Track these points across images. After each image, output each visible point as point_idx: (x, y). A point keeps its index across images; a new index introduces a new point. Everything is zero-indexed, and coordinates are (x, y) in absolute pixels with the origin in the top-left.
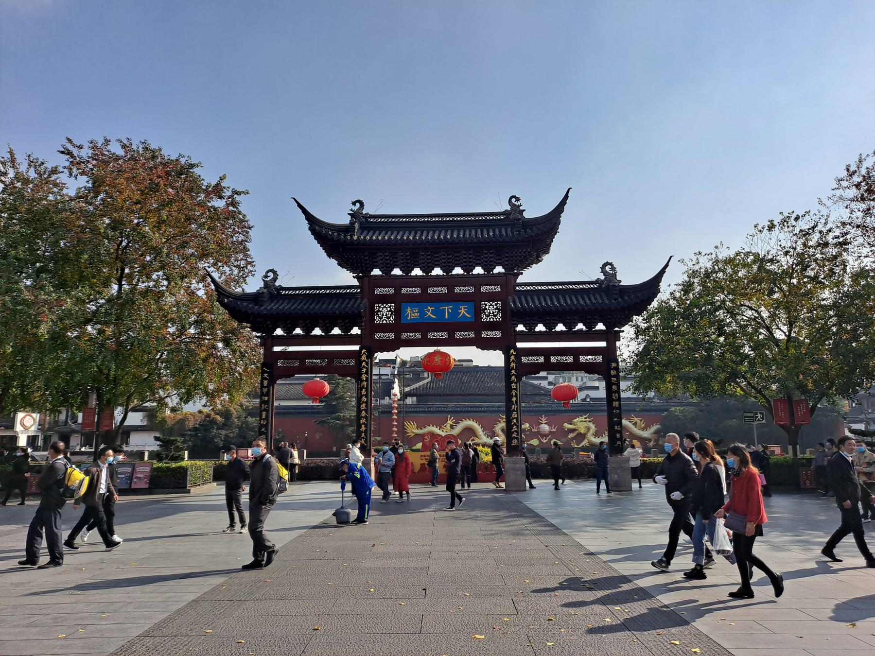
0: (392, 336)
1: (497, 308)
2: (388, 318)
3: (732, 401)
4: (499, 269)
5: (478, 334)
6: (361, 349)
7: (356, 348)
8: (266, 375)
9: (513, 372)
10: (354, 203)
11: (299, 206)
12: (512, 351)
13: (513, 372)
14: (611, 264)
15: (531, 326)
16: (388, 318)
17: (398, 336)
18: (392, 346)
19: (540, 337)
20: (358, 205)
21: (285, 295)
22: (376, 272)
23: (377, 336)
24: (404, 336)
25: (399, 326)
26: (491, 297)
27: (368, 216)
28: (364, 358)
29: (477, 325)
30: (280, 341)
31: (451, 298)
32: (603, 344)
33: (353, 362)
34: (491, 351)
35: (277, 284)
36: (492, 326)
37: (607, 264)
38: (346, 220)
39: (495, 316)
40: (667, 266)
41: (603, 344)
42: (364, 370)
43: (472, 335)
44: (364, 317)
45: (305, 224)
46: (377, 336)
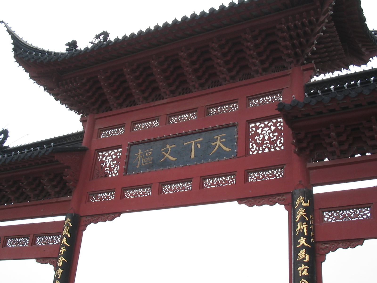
39: (273, 143)
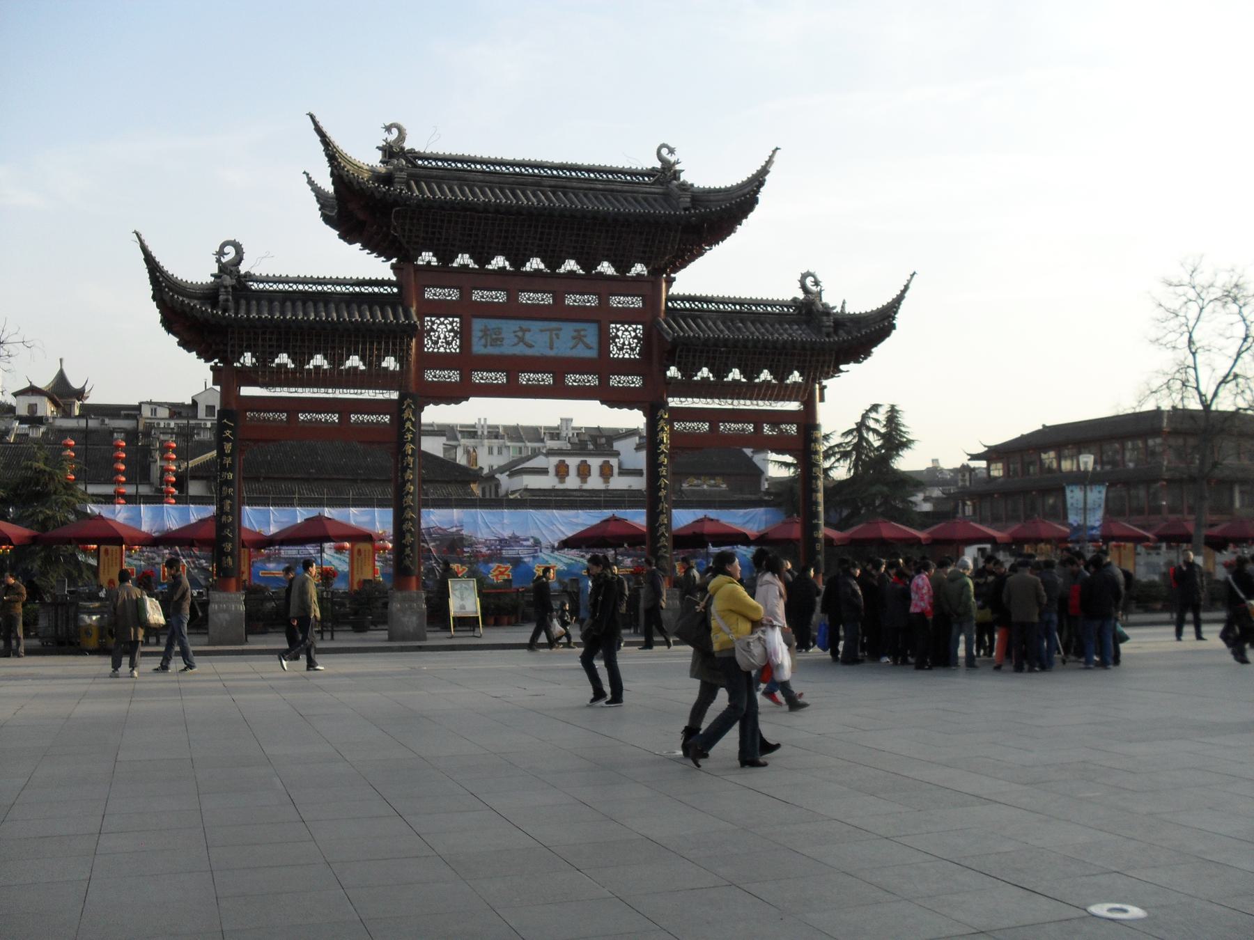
0: (454, 376)
1: (452, 330)
4: (639, 269)
5: (604, 380)
10: (388, 129)
11: (319, 130)
14: (813, 275)
15: (688, 370)
16: (448, 343)
17: (465, 377)
18: (454, 395)
20: (395, 131)
23: (430, 376)
24: (478, 377)
25: (465, 361)
26: (626, 317)
27: (412, 156)
29: (604, 365)
30: (249, 377)
31: (558, 314)
34: (625, 410)
36: (625, 367)
37: (808, 274)
39: (448, 343)
40: (906, 288)
42: (409, 436)
43: (592, 380)
44: (400, 337)
46: (430, 376)
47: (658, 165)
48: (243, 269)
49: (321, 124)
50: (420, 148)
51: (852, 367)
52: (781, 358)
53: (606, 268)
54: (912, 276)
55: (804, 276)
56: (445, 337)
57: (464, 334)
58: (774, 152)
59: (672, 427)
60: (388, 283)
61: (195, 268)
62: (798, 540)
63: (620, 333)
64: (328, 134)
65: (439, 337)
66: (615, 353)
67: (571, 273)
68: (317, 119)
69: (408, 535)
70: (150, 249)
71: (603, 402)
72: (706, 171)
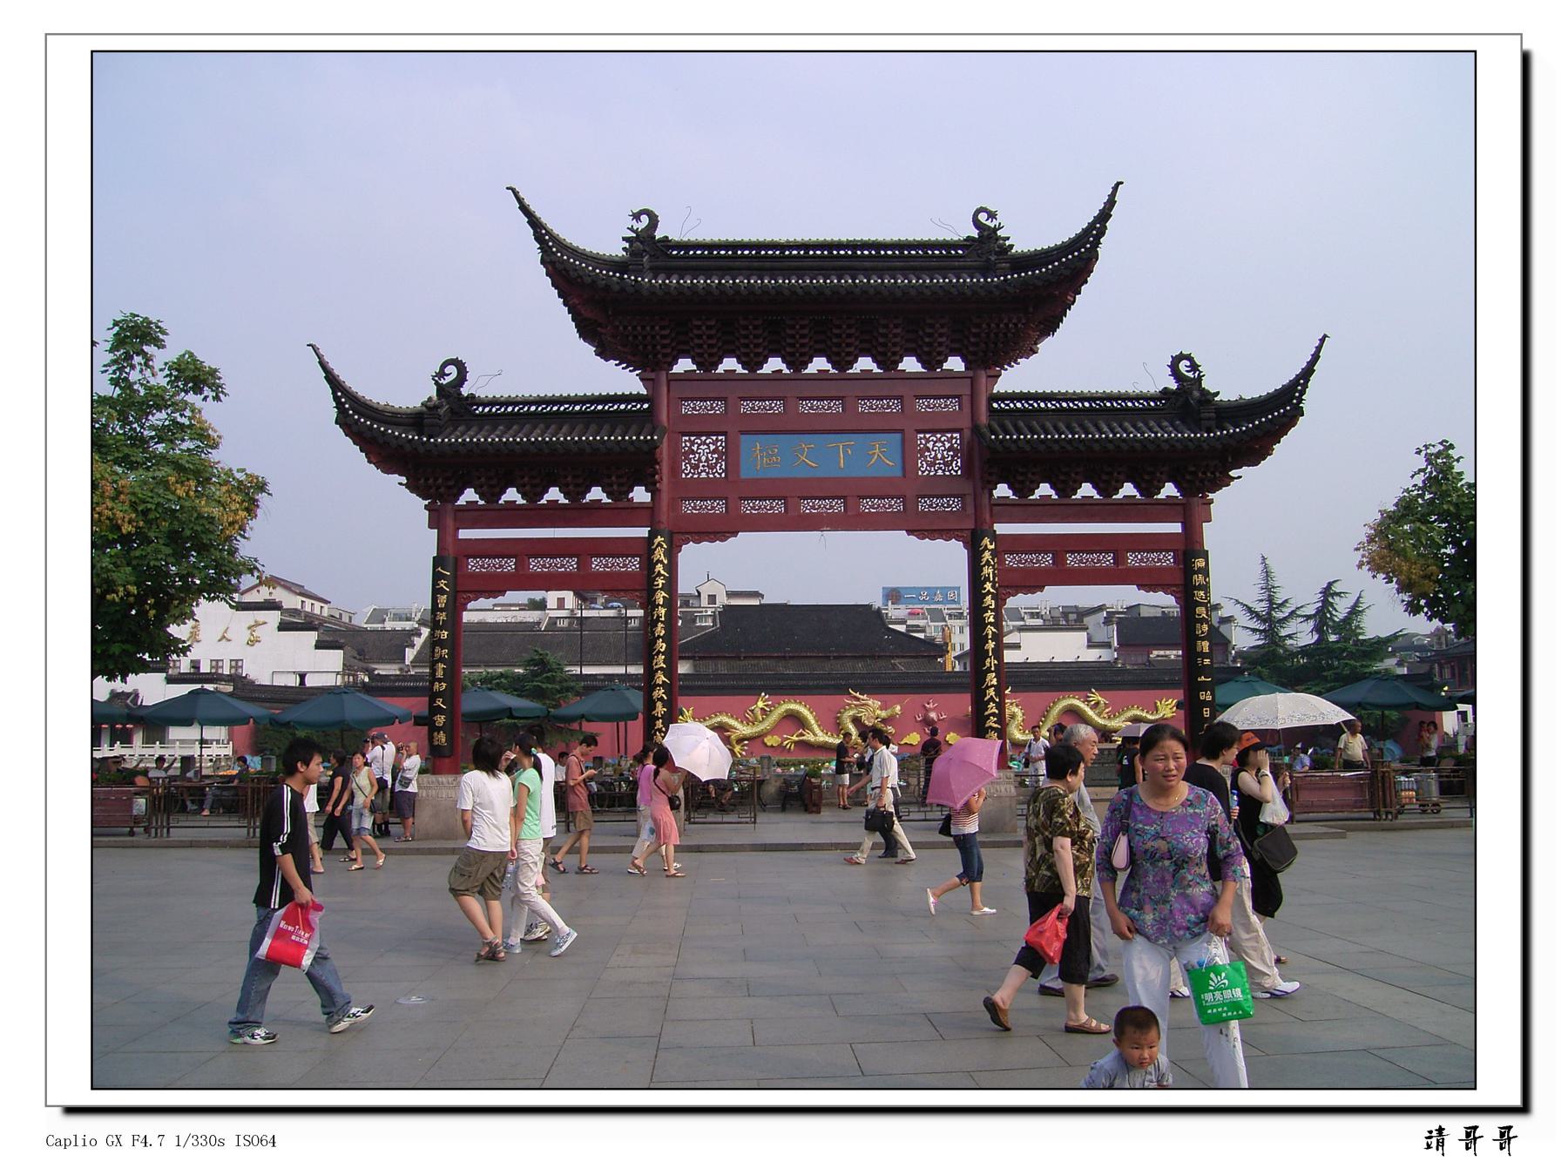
0: (719, 507)
2: (711, 467)
3: (113, 609)
6: (653, 535)
7: (643, 532)
8: (442, 584)
9: (988, 586)
10: (637, 216)
11: (524, 209)
12: (986, 541)
13: (988, 586)
14: (1189, 358)
16: (946, 464)
19: (512, 516)
21: (482, 415)
22: (684, 365)
23: (688, 508)
24: (748, 508)
28: (659, 554)
30: (473, 516)
32: (1176, 528)
33: (634, 564)
35: (465, 391)
37: (1181, 357)
38: (614, 247)
39: (711, 467)
40: (1316, 357)
41: (1176, 528)
42: (660, 582)
43: (896, 506)
44: (641, 466)
45: (533, 251)
46: (688, 508)
47: (975, 233)
48: (465, 391)
49: (527, 202)
50: (675, 236)
51: (1244, 471)
52: (1145, 465)
53: (910, 365)
54: (1322, 340)
55: (1177, 360)
56: (707, 460)
57: (729, 455)
58: (1115, 188)
59: (1001, 561)
60: (638, 398)
61: (407, 390)
62: (682, 658)
63: (930, 445)
64: (538, 214)
65: (699, 460)
66: (923, 469)
67: (866, 373)
68: (521, 195)
69: (659, 704)
70: (331, 365)
71: (910, 532)
72: (1032, 230)
